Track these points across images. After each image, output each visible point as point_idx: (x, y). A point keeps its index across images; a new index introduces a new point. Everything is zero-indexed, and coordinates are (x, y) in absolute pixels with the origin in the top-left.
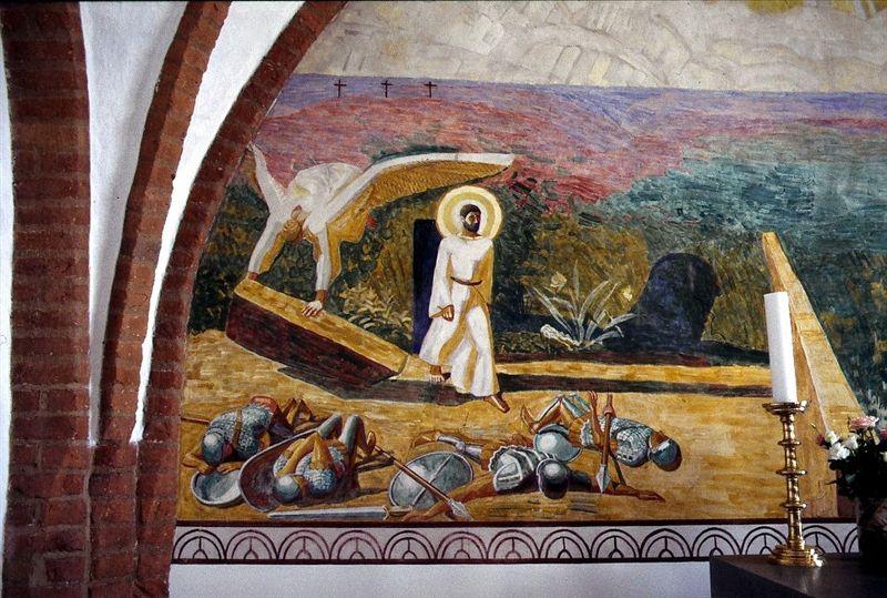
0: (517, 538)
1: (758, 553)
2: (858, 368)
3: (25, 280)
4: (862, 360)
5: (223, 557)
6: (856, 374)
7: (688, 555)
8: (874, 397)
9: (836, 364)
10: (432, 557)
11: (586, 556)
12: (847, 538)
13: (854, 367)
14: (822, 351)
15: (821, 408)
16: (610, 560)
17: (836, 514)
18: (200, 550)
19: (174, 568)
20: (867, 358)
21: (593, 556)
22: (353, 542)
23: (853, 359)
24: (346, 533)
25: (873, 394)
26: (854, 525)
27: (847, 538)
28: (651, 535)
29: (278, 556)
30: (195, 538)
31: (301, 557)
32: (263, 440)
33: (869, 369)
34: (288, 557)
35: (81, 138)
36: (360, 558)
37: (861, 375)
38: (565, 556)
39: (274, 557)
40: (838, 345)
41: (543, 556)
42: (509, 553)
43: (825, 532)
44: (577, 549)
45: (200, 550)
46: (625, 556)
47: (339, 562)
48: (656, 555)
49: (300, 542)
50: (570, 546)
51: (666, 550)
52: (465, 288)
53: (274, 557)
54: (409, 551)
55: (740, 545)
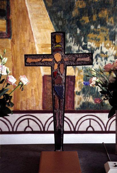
0: (31, 119)
1: (24, 131)
2: (62, 19)
4: (65, 14)
5: (42, 130)
6: (60, 23)
8: (71, 38)
9: (48, 17)
12: (47, 121)
13: (60, 19)
14: (39, 8)
15: (36, 46)
16: (25, 132)
17: (40, 108)
19: (65, 135)
20: (68, 12)
22: (27, 121)
23: (59, 13)
25: (70, 36)
26: (52, 115)
27: (47, 121)
32: (86, 67)
33: (69, 20)
34: (80, 130)
36: (31, 130)
37: (63, 24)
39: (104, 130)
40: (50, 4)
46: (95, 130)
48: (23, 130)
51: (29, 126)
53: (11, 130)
55: (75, 126)
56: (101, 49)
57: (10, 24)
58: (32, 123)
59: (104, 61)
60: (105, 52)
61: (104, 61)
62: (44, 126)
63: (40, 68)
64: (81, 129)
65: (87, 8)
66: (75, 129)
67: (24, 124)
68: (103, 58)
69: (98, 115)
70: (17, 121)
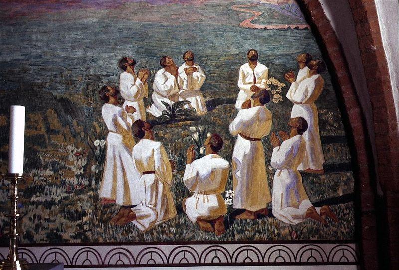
3: (28, 130)
5: (230, 261)
7: (293, 260)
10: (70, 264)
11: (325, 260)
18: (151, 259)
21: (234, 261)
24: (114, 249)
28: (111, 251)
29: (135, 262)
30: (85, 251)
31: (310, 260)
34: (142, 263)
35: (371, 22)
36: (186, 262)
38: (248, 260)
41: (202, 261)
42: (277, 258)
43: (91, 250)
44: (320, 256)
45: (151, 259)
47: (300, 263)
49: (309, 252)
50: (315, 253)
52: (248, 142)
53: (261, 261)
54: (311, 256)
55: (103, 259)
56: (3, 182)
57: (10, 142)
58: (219, 254)
59: (6, 194)
60: (7, 184)
61: (6, 194)
62: (200, 256)
63: (242, 206)
64: (143, 262)
65: (85, 153)
66: (72, 263)
67: (83, 257)
68: (5, 191)
69: (63, 248)
70: (97, 252)
